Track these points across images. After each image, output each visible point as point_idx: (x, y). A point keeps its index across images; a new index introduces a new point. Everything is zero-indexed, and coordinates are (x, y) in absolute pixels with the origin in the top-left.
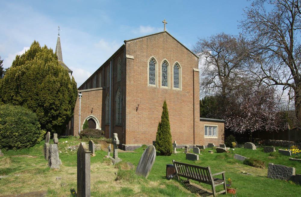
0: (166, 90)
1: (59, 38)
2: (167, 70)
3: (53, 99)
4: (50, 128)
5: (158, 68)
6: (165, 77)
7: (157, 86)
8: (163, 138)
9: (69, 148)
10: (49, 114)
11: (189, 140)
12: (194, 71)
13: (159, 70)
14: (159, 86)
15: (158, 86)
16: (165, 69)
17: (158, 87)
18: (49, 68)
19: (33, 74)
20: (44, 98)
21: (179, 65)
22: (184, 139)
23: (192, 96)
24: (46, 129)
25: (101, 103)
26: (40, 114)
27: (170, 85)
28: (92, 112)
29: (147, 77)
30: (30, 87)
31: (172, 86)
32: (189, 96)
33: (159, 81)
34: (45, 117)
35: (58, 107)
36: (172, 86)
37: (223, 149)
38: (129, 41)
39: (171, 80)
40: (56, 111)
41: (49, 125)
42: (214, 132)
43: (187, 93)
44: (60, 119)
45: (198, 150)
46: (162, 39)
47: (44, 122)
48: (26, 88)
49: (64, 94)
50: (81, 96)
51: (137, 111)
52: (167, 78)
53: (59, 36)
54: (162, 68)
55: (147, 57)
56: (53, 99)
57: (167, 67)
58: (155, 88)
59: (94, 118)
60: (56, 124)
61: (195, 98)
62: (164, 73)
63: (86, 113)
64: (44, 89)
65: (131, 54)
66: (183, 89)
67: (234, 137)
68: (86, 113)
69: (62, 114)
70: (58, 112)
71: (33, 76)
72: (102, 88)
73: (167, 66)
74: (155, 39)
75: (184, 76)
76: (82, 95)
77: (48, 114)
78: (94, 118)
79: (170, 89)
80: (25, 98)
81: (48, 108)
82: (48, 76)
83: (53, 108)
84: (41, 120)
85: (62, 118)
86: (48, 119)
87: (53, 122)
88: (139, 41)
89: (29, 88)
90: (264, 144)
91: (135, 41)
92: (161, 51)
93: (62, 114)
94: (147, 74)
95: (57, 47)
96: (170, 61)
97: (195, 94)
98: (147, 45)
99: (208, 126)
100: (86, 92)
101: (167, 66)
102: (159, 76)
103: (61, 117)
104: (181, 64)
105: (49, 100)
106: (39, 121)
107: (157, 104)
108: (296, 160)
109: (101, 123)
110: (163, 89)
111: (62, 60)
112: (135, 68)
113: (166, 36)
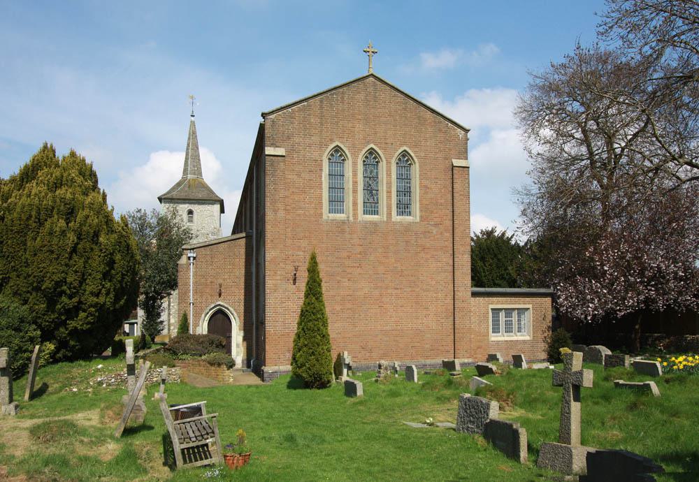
0: (375, 224)
1: (193, 124)
2: (377, 173)
3: (63, 272)
4: (65, 337)
5: (388, 173)
6: (371, 191)
7: (348, 217)
8: (306, 346)
9: (99, 379)
10: (59, 306)
11: (441, 348)
12: (453, 166)
13: (355, 174)
14: (355, 215)
15: (351, 215)
16: (371, 172)
17: (351, 219)
18: (55, 202)
19: (20, 219)
20: (41, 271)
21: (410, 156)
22: (427, 346)
23: (448, 234)
24: (56, 339)
25: (241, 272)
26: (37, 307)
27: (385, 209)
28: (220, 295)
29: (321, 198)
30: (14, 248)
31: (389, 214)
32: (441, 233)
33: (355, 204)
34: (50, 313)
35: (75, 288)
36: (389, 214)
37: (488, 367)
38: (272, 112)
39: (389, 197)
40: (70, 297)
41: (62, 330)
42: (519, 324)
43: (433, 228)
44: (82, 315)
45: (413, 371)
46: (361, 96)
47: (47, 324)
48: (5, 252)
49: (88, 258)
50: (194, 258)
51: (294, 284)
52: (377, 194)
53: (192, 118)
54: (365, 171)
55: (322, 146)
56: (63, 272)
57: (377, 165)
58: (343, 222)
59: (226, 308)
60: (76, 328)
61: (457, 239)
62: (371, 182)
63: (207, 299)
64: (41, 250)
65: (277, 144)
66: (421, 217)
67: (568, 335)
68: (207, 299)
69: (86, 303)
70: (75, 300)
71: (20, 225)
72: (244, 235)
73: (377, 162)
74: (343, 98)
75: (426, 182)
76: (195, 256)
77: (55, 307)
78: (226, 308)
79: (385, 219)
80: (5, 274)
81: (51, 293)
82: (49, 221)
83: (64, 292)
84: (39, 321)
85: (86, 314)
86: (57, 318)
87: (68, 324)
88: (300, 110)
89: (11, 252)
90: (672, 348)
91: (290, 110)
92: (359, 126)
93: (86, 303)
94: (321, 188)
95: (188, 145)
96: (385, 149)
97: (456, 226)
98: (322, 117)
99: (501, 310)
100: (205, 248)
101: (377, 162)
102: (355, 191)
103: (84, 311)
104: (415, 152)
105: (54, 273)
106: (35, 322)
107: (347, 262)
108: (626, 385)
109: (242, 318)
110: (366, 222)
111: (200, 174)
112: (290, 177)
113: (375, 85)
